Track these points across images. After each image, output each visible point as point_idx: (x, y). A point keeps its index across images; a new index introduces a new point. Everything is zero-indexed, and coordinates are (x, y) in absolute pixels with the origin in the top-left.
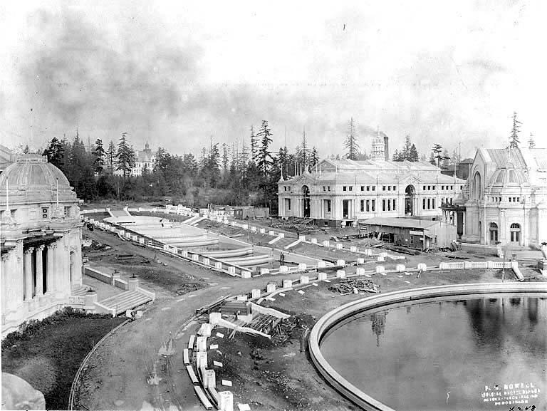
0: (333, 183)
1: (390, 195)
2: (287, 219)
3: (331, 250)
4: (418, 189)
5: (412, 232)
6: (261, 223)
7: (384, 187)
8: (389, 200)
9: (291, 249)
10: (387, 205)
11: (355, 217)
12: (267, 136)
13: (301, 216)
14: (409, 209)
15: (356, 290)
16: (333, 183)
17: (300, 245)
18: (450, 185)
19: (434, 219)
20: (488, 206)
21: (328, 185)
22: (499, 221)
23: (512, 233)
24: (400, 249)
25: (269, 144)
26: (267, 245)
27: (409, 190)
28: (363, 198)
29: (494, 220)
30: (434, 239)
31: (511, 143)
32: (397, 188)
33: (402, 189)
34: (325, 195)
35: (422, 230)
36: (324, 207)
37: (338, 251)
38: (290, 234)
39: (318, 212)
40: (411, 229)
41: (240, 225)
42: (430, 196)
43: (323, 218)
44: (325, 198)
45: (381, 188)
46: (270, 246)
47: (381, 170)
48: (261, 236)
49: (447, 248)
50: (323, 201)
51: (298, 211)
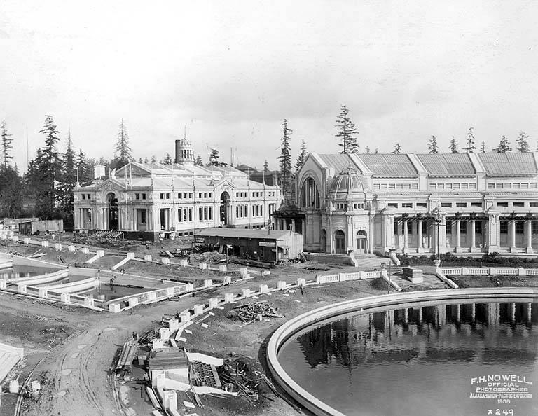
0: (150, 189)
1: (204, 203)
2: (86, 232)
3: (176, 268)
4: (232, 196)
5: (261, 244)
6: (58, 238)
7: (179, 195)
8: (205, 209)
9: (121, 269)
10: (205, 214)
11: (173, 229)
12: (54, 135)
13: (106, 229)
14: (223, 217)
15: (260, 316)
16: (150, 189)
17: (130, 263)
18: (260, 191)
19: (246, 228)
20: (334, 213)
21: (143, 193)
22: (347, 228)
23: (358, 240)
24: (250, 263)
25: (55, 145)
26: (86, 266)
27: (224, 196)
28: (180, 206)
29: (340, 227)
30: (285, 251)
31: (283, 150)
32: (213, 195)
33: (217, 197)
34: (139, 204)
35: (274, 241)
36: (137, 217)
37: (183, 269)
38: (114, 252)
39: (128, 223)
40: (262, 240)
41: (38, 243)
42: (243, 203)
43: (136, 230)
44: (139, 207)
45: (171, 196)
46: (92, 266)
47: (190, 175)
48: (73, 255)
49: (297, 259)
50: (135, 211)
51: (102, 224)
